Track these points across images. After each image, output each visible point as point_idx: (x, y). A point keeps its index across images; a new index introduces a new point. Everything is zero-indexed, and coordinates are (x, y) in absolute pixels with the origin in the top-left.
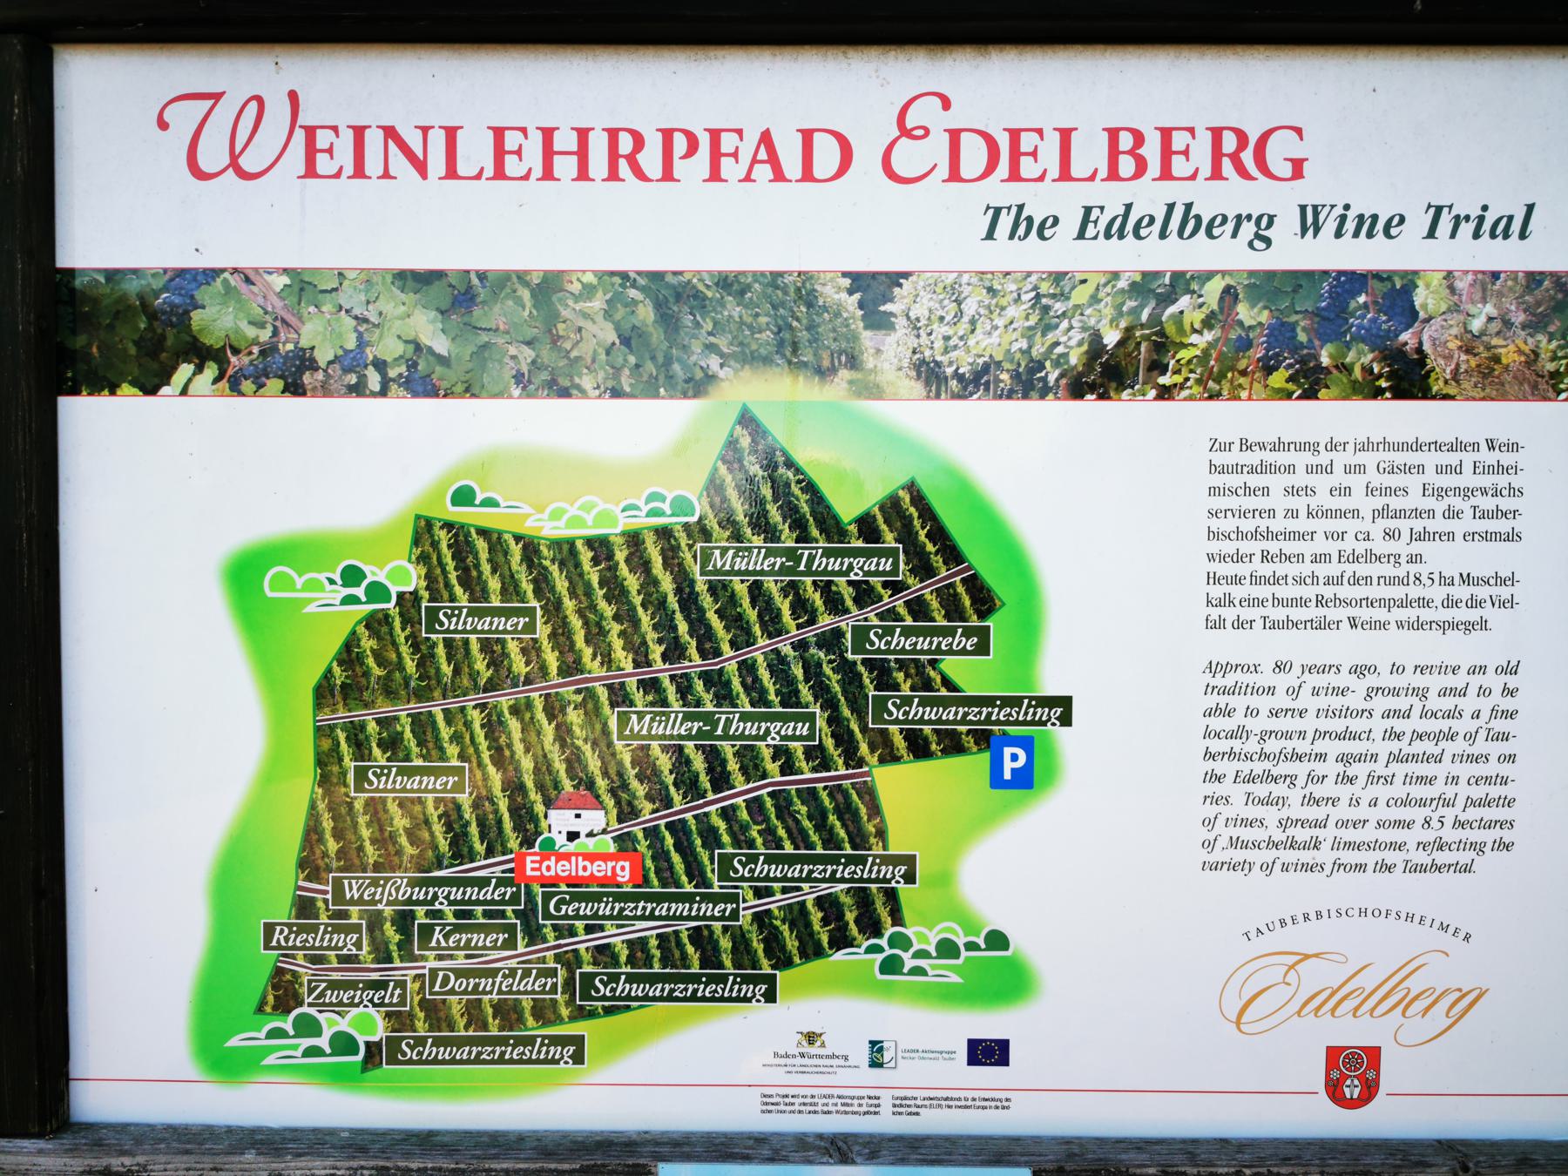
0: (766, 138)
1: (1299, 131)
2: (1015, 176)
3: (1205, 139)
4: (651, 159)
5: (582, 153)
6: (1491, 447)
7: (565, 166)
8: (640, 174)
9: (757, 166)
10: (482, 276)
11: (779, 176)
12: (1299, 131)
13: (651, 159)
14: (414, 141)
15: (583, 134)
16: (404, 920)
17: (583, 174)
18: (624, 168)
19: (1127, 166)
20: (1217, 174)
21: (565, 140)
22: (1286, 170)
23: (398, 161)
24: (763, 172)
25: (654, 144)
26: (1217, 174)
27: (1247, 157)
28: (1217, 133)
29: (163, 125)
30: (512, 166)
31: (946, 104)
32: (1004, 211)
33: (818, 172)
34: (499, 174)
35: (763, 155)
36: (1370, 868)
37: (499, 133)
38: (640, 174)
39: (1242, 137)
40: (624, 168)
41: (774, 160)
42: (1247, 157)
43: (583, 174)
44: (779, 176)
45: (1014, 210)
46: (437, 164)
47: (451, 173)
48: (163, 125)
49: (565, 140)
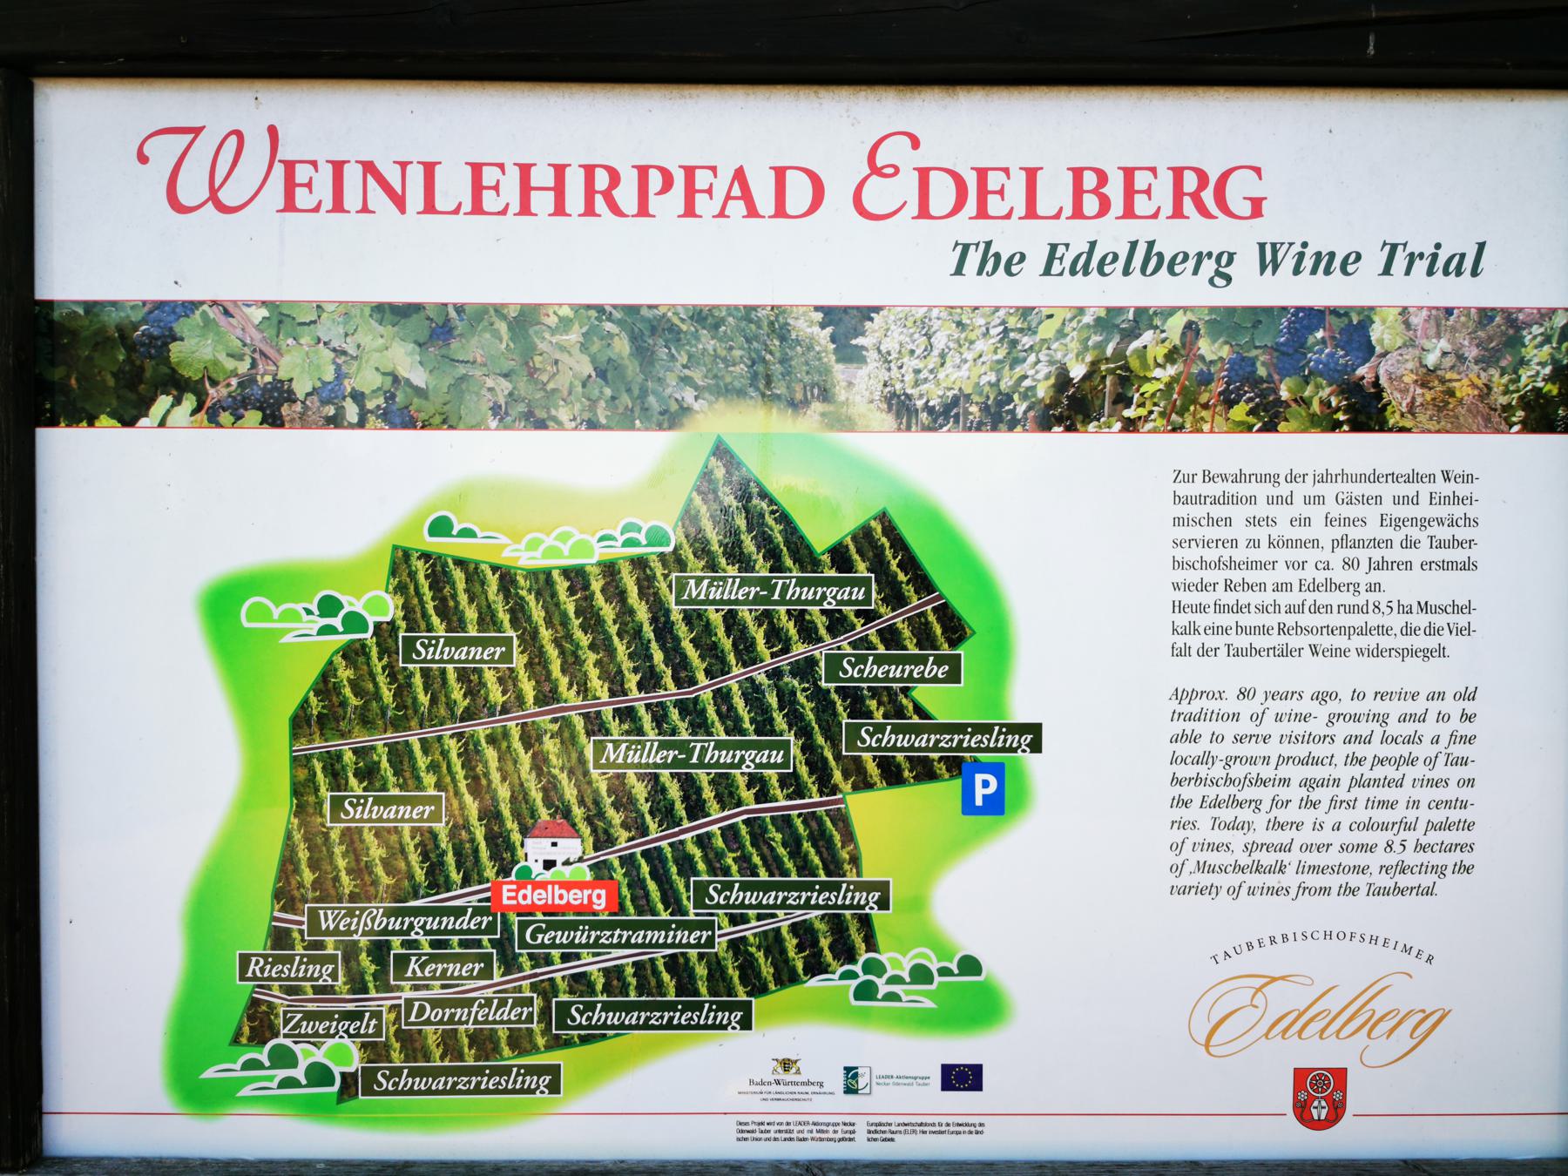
0: (740, 175)
1: (1258, 171)
2: (982, 213)
3: (1167, 178)
4: (626, 195)
5: (559, 189)
6: (1447, 478)
8: (615, 210)
9: (730, 202)
10: (460, 309)
11: (752, 212)
12: (1258, 171)
13: (626, 195)
14: (393, 176)
15: (560, 170)
16: (379, 951)
17: (560, 210)
18: (1188, 205)
19: (1091, 204)
20: (1178, 213)
21: (543, 176)
22: (1246, 208)
24: (737, 208)
25: (629, 181)
26: (1178, 213)
27: (1208, 196)
28: (1178, 173)
29: (143, 159)
30: (490, 201)
31: (915, 143)
32: (973, 248)
33: (934, 209)
34: (477, 209)
35: (736, 191)
36: (1334, 891)
37: (477, 169)
38: (615, 210)
39: (1202, 177)
40: (1188, 205)
41: (747, 196)
42: (1208, 196)
43: (560, 210)
44: (752, 212)
45: (982, 246)
46: (415, 198)
47: (430, 207)
48: (143, 159)
49: (543, 176)
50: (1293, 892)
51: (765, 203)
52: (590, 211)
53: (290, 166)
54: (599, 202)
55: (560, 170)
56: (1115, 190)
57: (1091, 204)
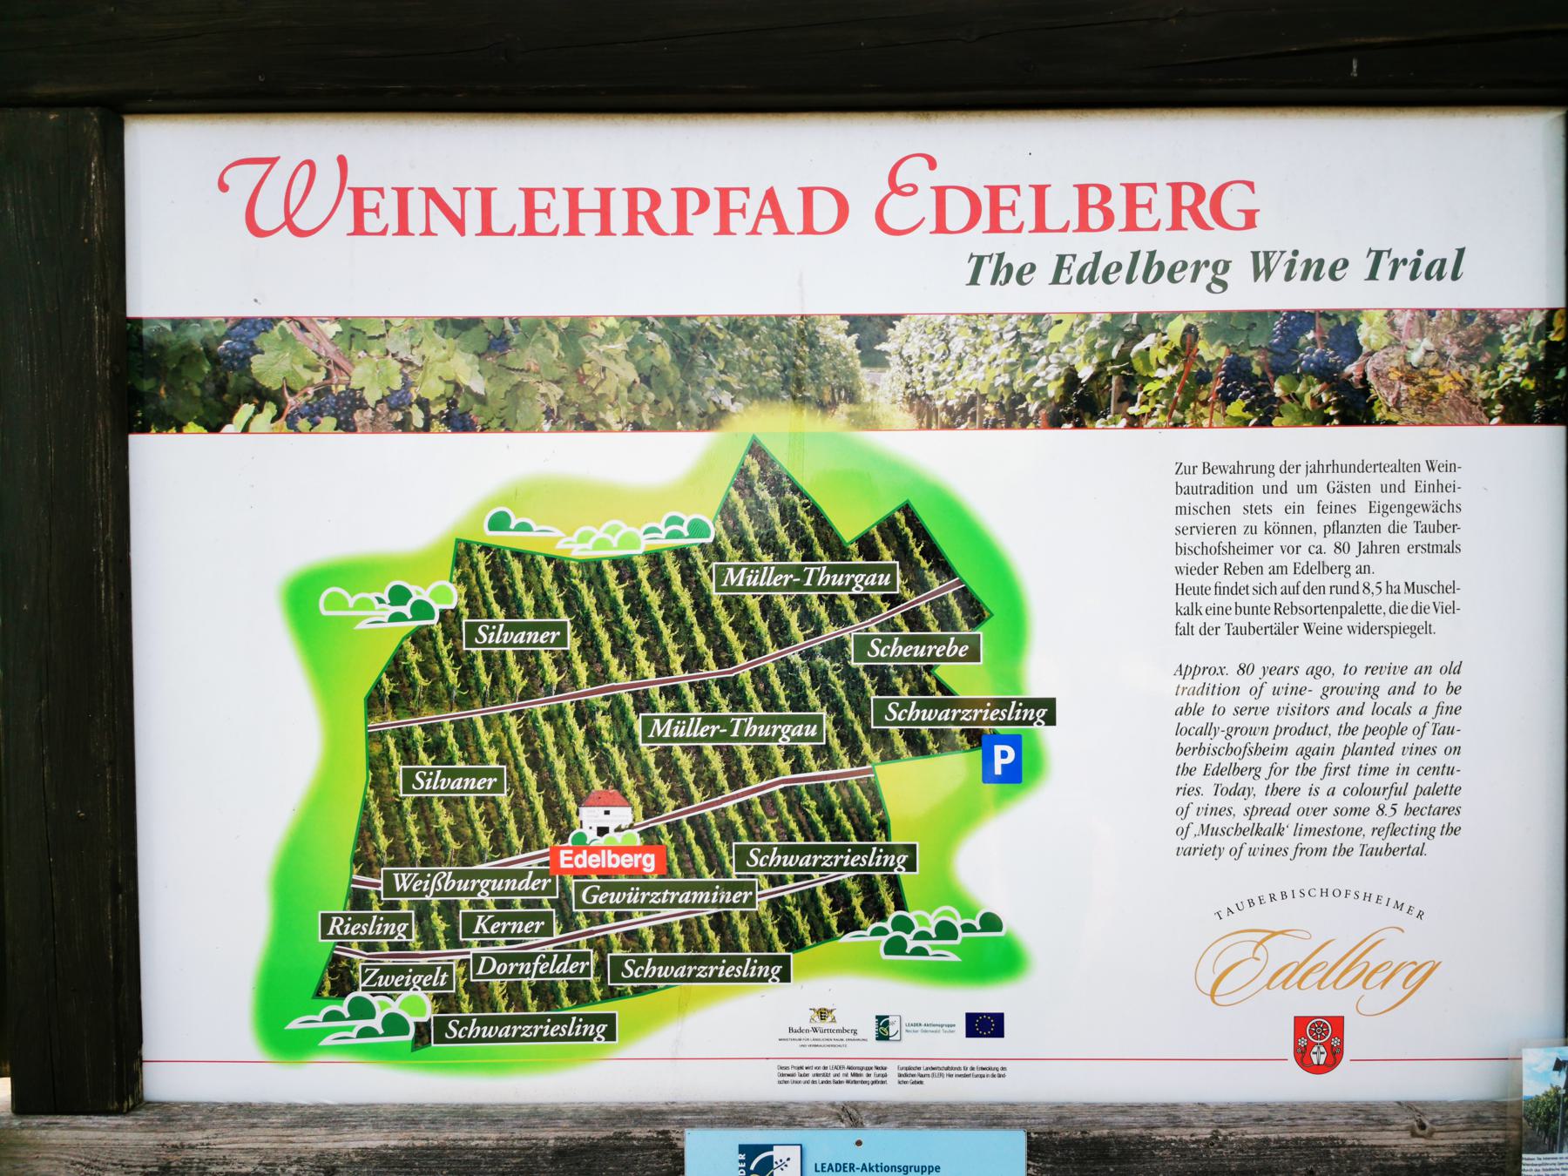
0: (770, 195)
2: (995, 227)
3: (1166, 194)
4: (667, 216)
5: (605, 212)
7: (590, 223)
8: (657, 229)
11: (782, 229)
13: (667, 216)
14: (454, 204)
15: (605, 194)
19: (1095, 218)
20: (1177, 225)
21: (589, 200)
22: (1240, 220)
23: (439, 220)
24: (768, 226)
26: (1177, 225)
27: (1205, 209)
28: (1176, 188)
29: (223, 187)
30: (541, 222)
31: (932, 164)
33: (817, 226)
34: (530, 230)
37: (529, 194)
38: (657, 229)
40: (642, 223)
41: (777, 215)
42: (1205, 209)
44: (782, 229)
48: (223, 187)
49: (589, 200)
50: (1291, 853)
51: (794, 220)
52: (633, 230)
53: (358, 193)
54: (642, 223)
55: (605, 194)
56: (1118, 204)
57: (1095, 218)
